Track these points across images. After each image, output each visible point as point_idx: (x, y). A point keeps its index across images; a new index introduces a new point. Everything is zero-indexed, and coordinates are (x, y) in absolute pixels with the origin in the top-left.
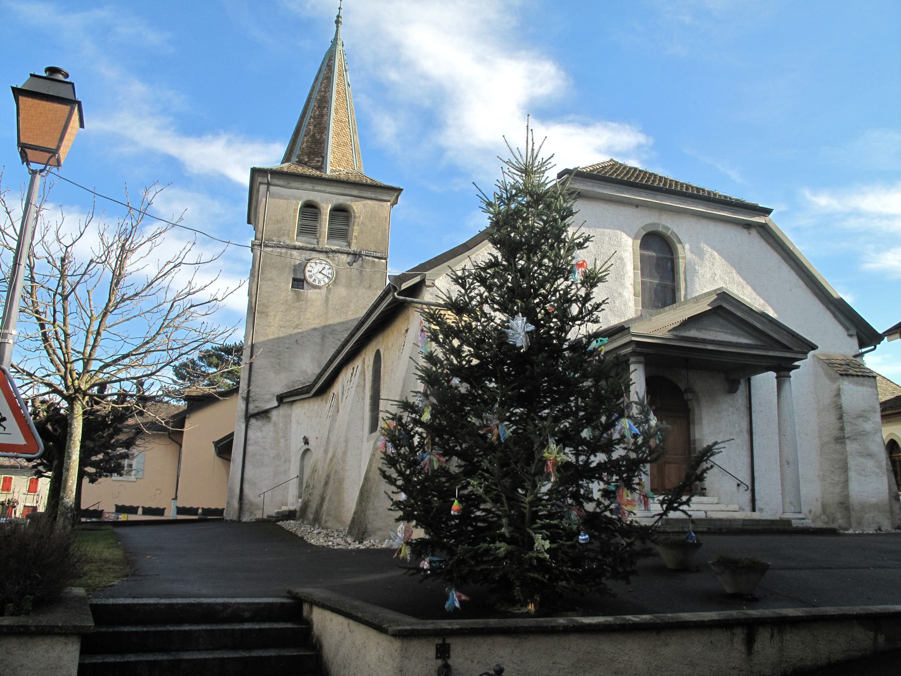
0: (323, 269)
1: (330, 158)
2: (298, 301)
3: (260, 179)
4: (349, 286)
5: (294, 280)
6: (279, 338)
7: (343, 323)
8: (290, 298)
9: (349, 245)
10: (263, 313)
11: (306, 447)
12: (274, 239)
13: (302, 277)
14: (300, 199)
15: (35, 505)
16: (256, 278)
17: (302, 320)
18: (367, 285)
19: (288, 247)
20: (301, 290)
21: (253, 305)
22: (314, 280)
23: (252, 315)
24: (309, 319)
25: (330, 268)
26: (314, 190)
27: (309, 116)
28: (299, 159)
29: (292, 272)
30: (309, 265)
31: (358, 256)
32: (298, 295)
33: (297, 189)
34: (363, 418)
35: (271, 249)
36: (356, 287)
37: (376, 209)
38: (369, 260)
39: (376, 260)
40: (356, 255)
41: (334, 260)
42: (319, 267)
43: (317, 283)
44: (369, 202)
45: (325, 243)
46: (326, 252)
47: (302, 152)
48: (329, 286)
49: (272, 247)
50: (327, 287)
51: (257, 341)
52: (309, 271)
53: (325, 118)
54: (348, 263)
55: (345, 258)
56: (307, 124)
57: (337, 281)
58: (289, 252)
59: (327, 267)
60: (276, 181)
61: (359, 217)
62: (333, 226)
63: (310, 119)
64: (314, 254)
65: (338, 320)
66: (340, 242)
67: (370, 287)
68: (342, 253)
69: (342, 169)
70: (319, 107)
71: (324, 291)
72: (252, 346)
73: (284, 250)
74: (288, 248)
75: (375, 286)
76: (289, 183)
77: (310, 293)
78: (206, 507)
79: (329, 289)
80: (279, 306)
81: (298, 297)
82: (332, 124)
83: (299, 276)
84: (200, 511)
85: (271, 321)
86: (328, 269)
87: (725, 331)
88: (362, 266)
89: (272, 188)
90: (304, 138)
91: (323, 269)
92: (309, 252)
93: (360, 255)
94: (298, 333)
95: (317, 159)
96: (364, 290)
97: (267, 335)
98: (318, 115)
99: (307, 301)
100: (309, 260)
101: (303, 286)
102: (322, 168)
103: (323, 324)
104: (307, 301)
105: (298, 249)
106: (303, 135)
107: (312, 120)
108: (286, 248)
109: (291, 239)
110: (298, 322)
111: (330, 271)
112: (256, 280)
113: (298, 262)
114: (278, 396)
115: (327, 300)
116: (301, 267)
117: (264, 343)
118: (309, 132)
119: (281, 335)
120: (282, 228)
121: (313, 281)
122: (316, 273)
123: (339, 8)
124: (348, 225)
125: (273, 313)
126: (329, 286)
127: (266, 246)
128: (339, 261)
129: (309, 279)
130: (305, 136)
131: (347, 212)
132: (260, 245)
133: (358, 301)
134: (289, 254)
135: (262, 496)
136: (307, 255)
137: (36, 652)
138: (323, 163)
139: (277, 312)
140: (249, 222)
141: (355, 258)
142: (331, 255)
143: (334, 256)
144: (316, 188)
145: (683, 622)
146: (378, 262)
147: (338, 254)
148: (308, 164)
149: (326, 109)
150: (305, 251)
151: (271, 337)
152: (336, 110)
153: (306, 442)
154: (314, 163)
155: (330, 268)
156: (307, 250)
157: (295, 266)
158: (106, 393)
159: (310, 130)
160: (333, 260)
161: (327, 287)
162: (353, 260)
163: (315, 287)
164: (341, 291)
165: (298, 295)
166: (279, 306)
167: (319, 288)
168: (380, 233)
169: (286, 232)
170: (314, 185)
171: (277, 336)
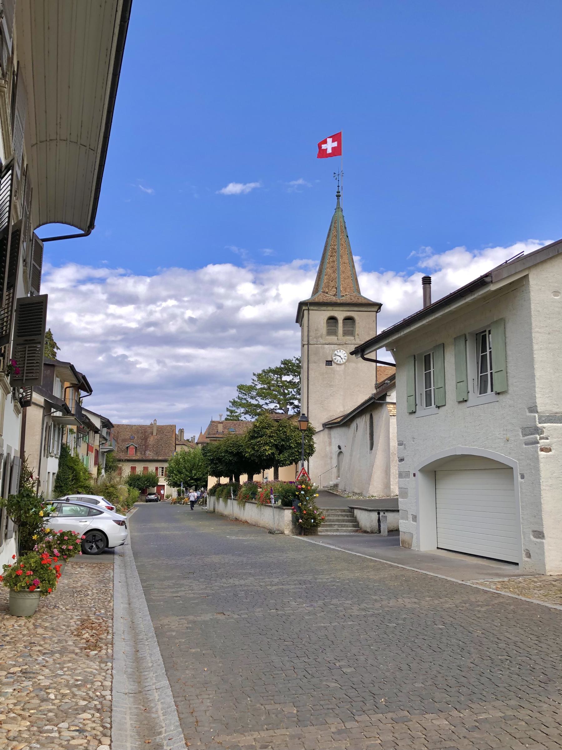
3: (304, 308)
11: (340, 451)
13: (331, 360)
26: (332, 310)
34: (367, 442)
43: (339, 362)
83: (330, 359)
114: (323, 424)
135: (320, 477)
140: (297, 322)
153: (339, 447)
160: (347, 348)
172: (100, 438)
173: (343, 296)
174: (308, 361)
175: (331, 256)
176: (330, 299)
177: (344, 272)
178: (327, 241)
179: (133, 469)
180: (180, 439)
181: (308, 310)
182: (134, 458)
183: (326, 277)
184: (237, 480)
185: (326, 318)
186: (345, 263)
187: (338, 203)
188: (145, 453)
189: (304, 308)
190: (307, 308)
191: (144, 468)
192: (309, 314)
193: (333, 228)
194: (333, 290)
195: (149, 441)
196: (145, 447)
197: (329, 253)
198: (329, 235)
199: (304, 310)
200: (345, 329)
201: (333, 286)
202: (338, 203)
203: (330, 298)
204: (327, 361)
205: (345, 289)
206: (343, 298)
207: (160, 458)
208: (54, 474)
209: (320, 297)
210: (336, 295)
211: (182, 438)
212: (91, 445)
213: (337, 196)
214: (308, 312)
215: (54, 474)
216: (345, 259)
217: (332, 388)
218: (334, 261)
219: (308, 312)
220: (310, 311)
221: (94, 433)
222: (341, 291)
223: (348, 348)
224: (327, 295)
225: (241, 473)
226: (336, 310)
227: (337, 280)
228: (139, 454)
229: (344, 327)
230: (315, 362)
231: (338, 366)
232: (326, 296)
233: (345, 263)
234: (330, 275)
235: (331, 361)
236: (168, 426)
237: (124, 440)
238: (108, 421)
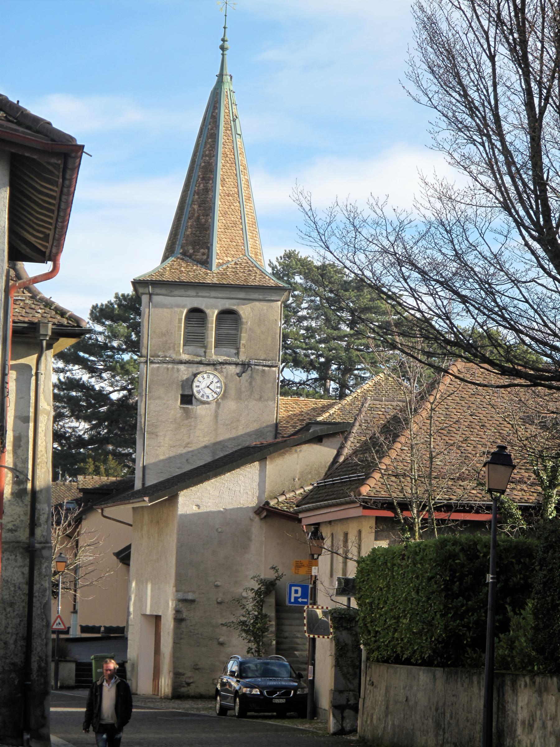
0: (211, 383)
1: (216, 248)
2: (187, 419)
4: (239, 398)
5: (183, 396)
6: (170, 458)
7: (234, 439)
8: (179, 415)
9: (237, 354)
10: (153, 433)
12: (160, 354)
13: (190, 393)
14: (184, 307)
16: (144, 397)
17: (191, 438)
18: (257, 397)
19: (174, 362)
20: (190, 407)
21: (143, 426)
22: (203, 396)
23: (142, 436)
24: (198, 437)
25: (218, 382)
27: (196, 177)
28: (184, 250)
29: (181, 389)
30: (196, 380)
31: (247, 366)
32: (187, 413)
33: (180, 296)
35: (157, 365)
36: (246, 400)
37: (265, 311)
38: (258, 369)
39: (266, 369)
40: (245, 366)
41: (222, 372)
42: (207, 382)
43: (205, 399)
44: (257, 303)
45: (213, 355)
46: (214, 365)
47: (186, 240)
48: (218, 400)
49: (158, 363)
50: (216, 402)
51: (148, 462)
52: (197, 386)
53: (211, 194)
54: (237, 374)
55: (233, 369)
56: (190, 203)
57: (226, 395)
58: (175, 366)
59: (215, 380)
60: (157, 290)
61: (247, 322)
62: (221, 332)
63: (194, 195)
64: (201, 368)
65: (227, 436)
66: (229, 350)
67: (261, 398)
68: (230, 364)
70: (203, 179)
71: (213, 406)
72: (144, 467)
73: (170, 366)
74: (174, 363)
75: (266, 397)
76: (171, 291)
77: (198, 410)
78: (108, 625)
79: (218, 404)
80: (169, 425)
81: (187, 413)
82: (218, 203)
84: (102, 629)
85: (161, 441)
86: (216, 383)
88: (251, 377)
89: (155, 298)
90: (188, 222)
91: (211, 383)
92: (196, 365)
93: (249, 365)
94: (189, 452)
95: (202, 250)
96: (254, 402)
97: (158, 455)
98: (203, 190)
99: (196, 418)
100: (195, 375)
102: (208, 263)
103: (213, 441)
104: (196, 418)
105: (185, 363)
106: (187, 218)
107: (196, 197)
108: (172, 363)
109: (177, 353)
110: (188, 441)
111: (219, 385)
112: (144, 399)
113: (185, 377)
115: (216, 416)
116: (188, 383)
117: (155, 464)
118: (193, 214)
119: (172, 454)
120: (167, 341)
121: (202, 397)
122: (204, 388)
123: (225, 28)
124: (237, 329)
125: (163, 433)
126: (218, 400)
127: (152, 362)
128: (227, 373)
129: (202, 399)
130: (189, 218)
131: (236, 314)
132: (146, 362)
133: (248, 414)
134: (175, 369)
136: (194, 369)
138: (208, 257)
139: (166, 431)
141: (244, 368)
142: (219, 367)
143: (221, 368)
145: (25, 238)
146: (269, 371)
147: (225, 366)
148: (193, 257)
149: (211, 182)
150: (191, 365)
151: (162, 458)
152: (223, 180)
154: (199, 256)
155: (218, 382)
156: (193, 363)
157: (183, 381)
159: (194, 210)
160: (221, 372)
161: (216, 402)
162: (242, 371)
163: (204, 403)
164: (231, 405)
165: (186, 411)
166: (169, 425)
167: (208, 403)
168: (270, 339)
169: (172, 345)
171: (167, 456)
223: (224, 370)
226: (202, 297)
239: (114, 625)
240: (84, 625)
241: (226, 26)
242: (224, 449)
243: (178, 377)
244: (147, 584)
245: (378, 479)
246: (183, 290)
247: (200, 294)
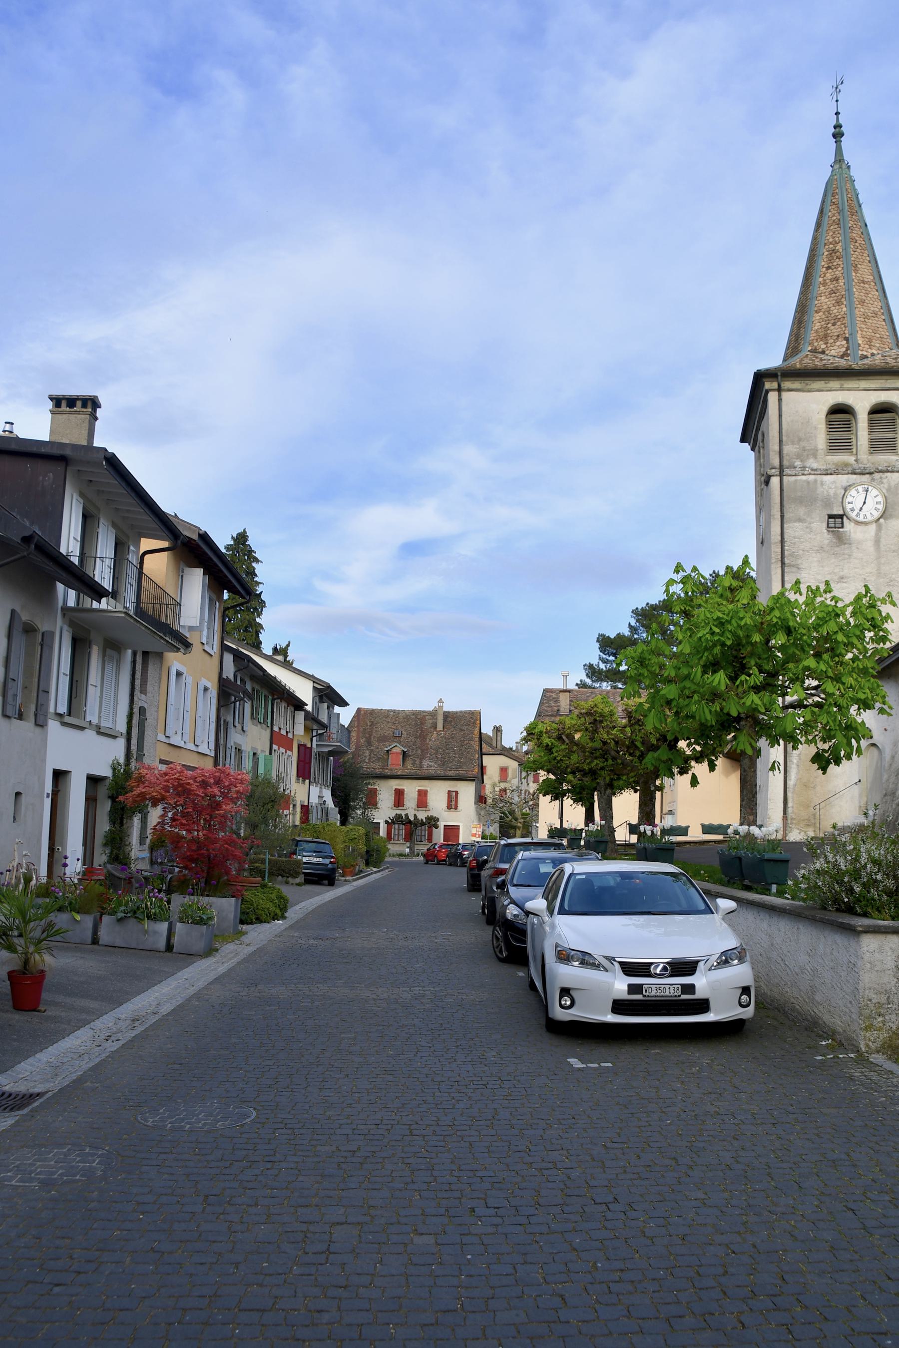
8: (826, 542)
13: (841, 512)
15: (174, 951)
26: (842, 389)
69: (875, 352)
83: (837, 511)
87: (47, 545)
99: (850, 544)
100: (846, 489)
101: (842, 523)
104: (850, 544)
115: (877, 541)
128: (889, 484)
137: (836, 520)
140: (743, 440)
144: (846, 386)
158: (110, 591)
170: (843, 382)
172: (305, 719)
173: (866, 357)
174: (782, 517)
175: (828, 268)
176: (832, 363)
177: (862, 302)
178: (815, 239)
179: (399, 796)
180: (494, 745)
181: (779, 390)
182: (400, 772)
183: (817, 317)
184: (607, 813)
185: (825, 410)
186: (863, 282)
187: (839, 151)
188: (421, 763)
189: (767, 385)
190: (775, 385)
191: (419, 791)
192: (780, 400)
193: (828, 207)
194: (838, 343)
195: (430, 740)
196: (422, 751)
197: (822, 262)
198: (818, 225)
199: (767, 392)
200: (876, 436)
201: (838, 336)
202: (839, 151)
203: (833, 355)
204: (830, 516)
205: (869, 342)
206: (866, 361)
207: (451, 773)
208: (93, 781)
209: (806, 361)
210: (848, 355)
211: (499, 743)
212: (283, 732)
213: (834, 136)
214: (780, 395)
215: (93, 781)
216: (865, 271)
217: (845, 585)
218: (836, 279)
219: (780, 395)
220: (785, 395)
221: (292, 709)
222: (859, 345)
223: (885, 481)
224: (822, 356)
225: (612, 788)
226: (849, 389)
227: (847, 321)
228: (409, 765)
229: (871, 430)
230: (800, 520)
231: (860, 528)
232: (821, 360)
233: (863, 282)
234: (829, 311)
235: (841, 517)
236: (465, 712)
237: (383, 739)
238: (329, 687)
239: (716, 823)
240: (706, 823)
241: (839, 111)
242: (891, 583)
243: (823, 492)
244: (88, 873)
245: (163, 927)
246: (823, 382)
247: (846, 386)
